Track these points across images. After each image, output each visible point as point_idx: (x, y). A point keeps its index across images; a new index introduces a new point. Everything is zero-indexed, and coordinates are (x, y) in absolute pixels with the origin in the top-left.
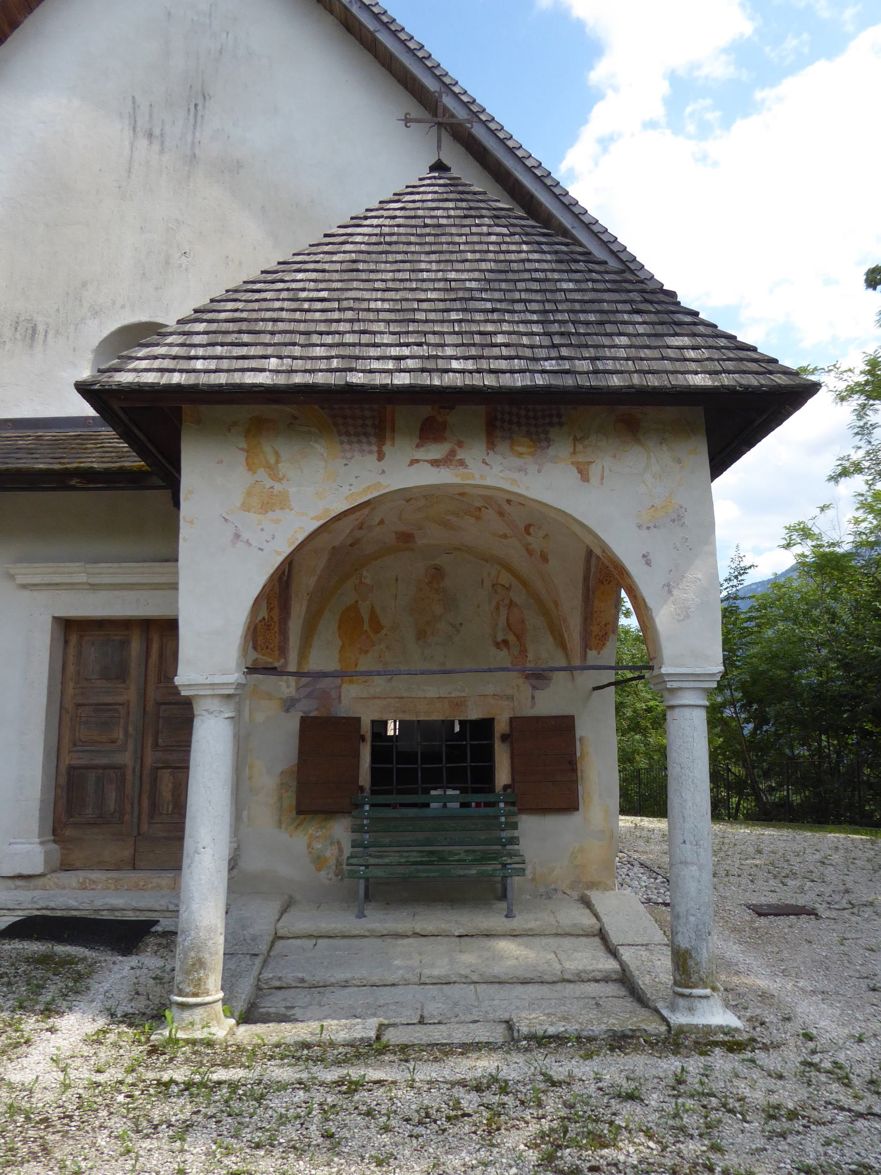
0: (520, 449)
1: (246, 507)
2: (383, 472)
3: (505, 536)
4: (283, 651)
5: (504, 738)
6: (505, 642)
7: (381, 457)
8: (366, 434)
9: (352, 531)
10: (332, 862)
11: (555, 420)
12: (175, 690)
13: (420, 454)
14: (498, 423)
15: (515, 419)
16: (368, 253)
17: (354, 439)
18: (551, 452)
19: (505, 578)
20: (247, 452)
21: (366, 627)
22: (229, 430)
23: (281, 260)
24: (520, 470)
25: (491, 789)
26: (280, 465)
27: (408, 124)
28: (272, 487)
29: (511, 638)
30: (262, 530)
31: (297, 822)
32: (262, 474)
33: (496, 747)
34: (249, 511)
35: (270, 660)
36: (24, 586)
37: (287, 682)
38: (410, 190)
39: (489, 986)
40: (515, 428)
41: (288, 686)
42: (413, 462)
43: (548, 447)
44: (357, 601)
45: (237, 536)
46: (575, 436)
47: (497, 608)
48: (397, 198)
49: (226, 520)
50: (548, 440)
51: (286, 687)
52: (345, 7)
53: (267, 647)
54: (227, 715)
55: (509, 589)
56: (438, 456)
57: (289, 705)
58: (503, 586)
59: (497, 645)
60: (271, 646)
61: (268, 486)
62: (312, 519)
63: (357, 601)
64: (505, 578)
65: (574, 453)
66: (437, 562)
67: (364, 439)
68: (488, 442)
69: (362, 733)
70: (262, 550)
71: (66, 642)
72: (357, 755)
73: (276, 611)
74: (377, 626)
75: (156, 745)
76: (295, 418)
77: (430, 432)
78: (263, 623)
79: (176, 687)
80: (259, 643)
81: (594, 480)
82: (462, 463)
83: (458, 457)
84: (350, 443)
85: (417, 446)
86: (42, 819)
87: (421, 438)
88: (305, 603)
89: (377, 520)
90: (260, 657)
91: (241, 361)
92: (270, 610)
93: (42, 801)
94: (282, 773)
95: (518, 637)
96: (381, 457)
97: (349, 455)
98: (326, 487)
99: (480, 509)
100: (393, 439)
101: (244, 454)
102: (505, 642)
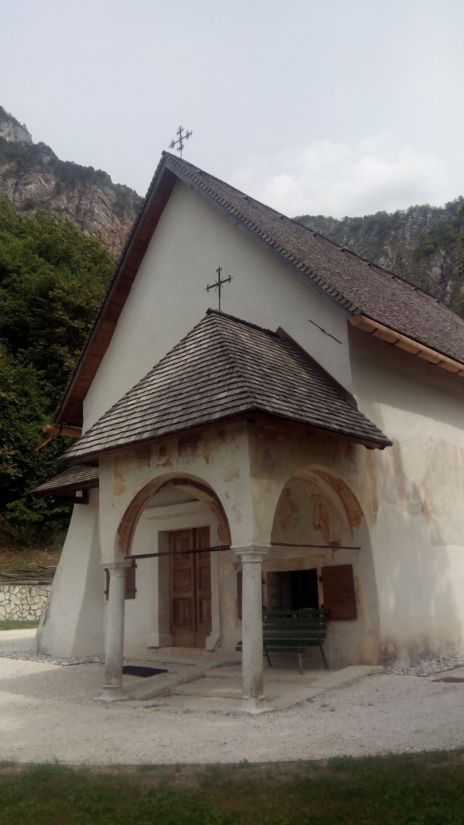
6: (319, 526)
29: (322, 524)
36: (149, 519)
39: (225, 699)
42: (158, 466)
48: (183, 342)
50: (197, 447)
71: (170, 542)
75: (200, 588)
77: (163, 452)
81: (210, 462)
82: (171, 464)
95: (325, 522)
102: (319, 526)
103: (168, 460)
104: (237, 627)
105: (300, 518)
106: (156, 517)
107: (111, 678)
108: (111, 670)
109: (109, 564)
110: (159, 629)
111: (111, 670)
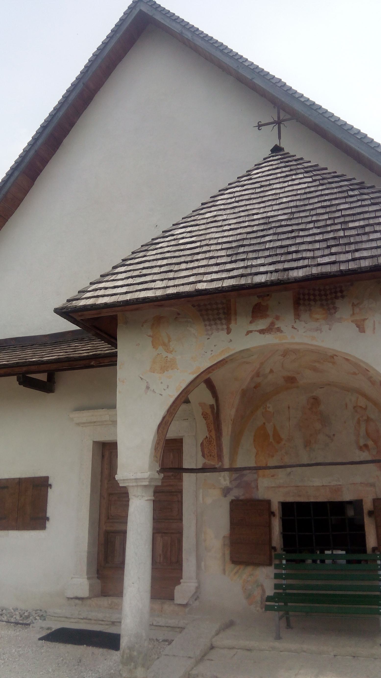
0: (317, 316)
1: (152, 370)
2: (231, 341)
3: (355, 374)
4: (220, 457)
5: (371, 513)
6: (366, 446)
7: (229, 331)
8: (220, 319)
9: (252, 378)
10: (258, 598)
11: (339, 294)
12: (117, 483)
13: (253, 327)
14: (301, 302)
15: (312, 297)
16: (224, 209)
17: (213, 322)
18: (337, 315)
19: (362, 402)
20: (152, 337)
21: (271, 440)
22: (143, 326)
23: (175, 223)
24: (317, 330)
25: (364, 550)
26: (171, 343)
27: (260, 128)
28: (167, 357)
30: (162, 383)
31: (235, 570)
32: (161, 349)
33: (365, 520)
34: (154, 373)
35: (213, 463)
36: (78, 424)
37: (224, 477)
38: (257, 167)
40: (312, 303)
41: (225, 480)
42: (249, 332)
43: (335, 313)
44: (264, 423)
45: (148, 388)
46: (353, 303)
47: (359, 422)
49: (142, 379)
50: (335, 308)
51: (224, 480)
52: (235, 70)
53: (210, 455)
54: (146, 499)
55: (365, 409)
56: (264, 327)
57: (226, 492)
58: (361, 407)
59: (360, 448)
60: (213, 454)
61: (164, 356)
62: (190, 374)
63: (264, 423)
64: (362, 402)
65: (353, 314)
66: (314, 394)
67: (218, 322)
68: (295, 315)
69: (272, 511)
70: (161, 395)
71: (103, 456)
72: (269, 525)
73: (213, 433)
74: (278, 439)
76: (179, 314)
77: (258, 311)
78: (207, 440)
79: (116, 481)
80: (206, 453)
82: (279, 330)
83: (276, 326)
84: (210, 325)
85: (251, 322)
86: (89, 563)
87: (253, 317)
88: (230, 427)
89: (268, 370)
90: (207, 461)
91: (141, 285)
92: (210, 431)
93: (89, 553)
94: (224, 537)
96: (229, 331)
97: (210, 332)
98: (196, 352)
99: (333, 357)
100: (236, 319)
101: (150, 339)
102: (366, 446)
103: (273, 324)
104: (224, 573)
105: (334, 435)
106: (91, 422)
107: (135, 668)
108: (135, 653)
109: (136, 479)
110: (87, 573)
111: (135, 653)
